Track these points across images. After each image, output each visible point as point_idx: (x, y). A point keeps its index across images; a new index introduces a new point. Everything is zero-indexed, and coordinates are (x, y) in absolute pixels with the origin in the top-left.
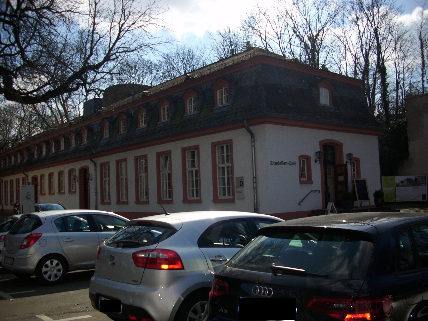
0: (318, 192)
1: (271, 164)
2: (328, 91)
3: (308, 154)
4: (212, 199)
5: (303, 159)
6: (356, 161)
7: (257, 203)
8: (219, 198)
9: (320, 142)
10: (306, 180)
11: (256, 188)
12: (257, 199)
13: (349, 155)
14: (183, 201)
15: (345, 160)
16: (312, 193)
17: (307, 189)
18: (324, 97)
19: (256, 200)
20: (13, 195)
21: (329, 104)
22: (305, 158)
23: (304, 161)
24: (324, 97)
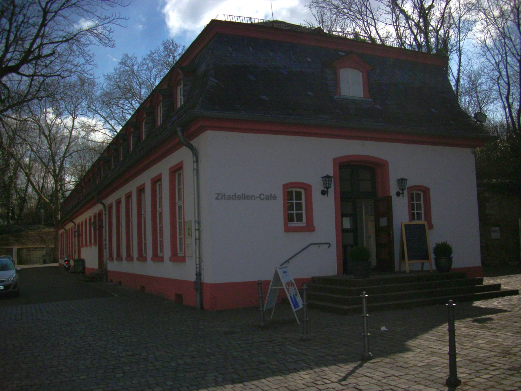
0: (328, 245)
1: (217, 199)
2: (361, 74)
3: (310, 183)
4: (170, 256)
5: (418, 192)
6: (424, 192)
7: (200, 264)
8: (179, 255)
9: (335, 160)
10: (305, 225)
11: (199, 239)
12: (199, 258)
13: (402, 181)
14: (170, 258)
15: (393, 188)
16: (312, 246)
17: (301, 240)
18: (351, 84)
19: (198, 260)
20: (162, 242)
21: (362, 96)
22: (421, 190)
23: (300, 193)
24: (351, 84)
